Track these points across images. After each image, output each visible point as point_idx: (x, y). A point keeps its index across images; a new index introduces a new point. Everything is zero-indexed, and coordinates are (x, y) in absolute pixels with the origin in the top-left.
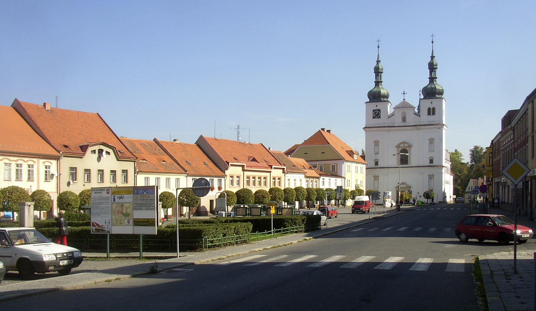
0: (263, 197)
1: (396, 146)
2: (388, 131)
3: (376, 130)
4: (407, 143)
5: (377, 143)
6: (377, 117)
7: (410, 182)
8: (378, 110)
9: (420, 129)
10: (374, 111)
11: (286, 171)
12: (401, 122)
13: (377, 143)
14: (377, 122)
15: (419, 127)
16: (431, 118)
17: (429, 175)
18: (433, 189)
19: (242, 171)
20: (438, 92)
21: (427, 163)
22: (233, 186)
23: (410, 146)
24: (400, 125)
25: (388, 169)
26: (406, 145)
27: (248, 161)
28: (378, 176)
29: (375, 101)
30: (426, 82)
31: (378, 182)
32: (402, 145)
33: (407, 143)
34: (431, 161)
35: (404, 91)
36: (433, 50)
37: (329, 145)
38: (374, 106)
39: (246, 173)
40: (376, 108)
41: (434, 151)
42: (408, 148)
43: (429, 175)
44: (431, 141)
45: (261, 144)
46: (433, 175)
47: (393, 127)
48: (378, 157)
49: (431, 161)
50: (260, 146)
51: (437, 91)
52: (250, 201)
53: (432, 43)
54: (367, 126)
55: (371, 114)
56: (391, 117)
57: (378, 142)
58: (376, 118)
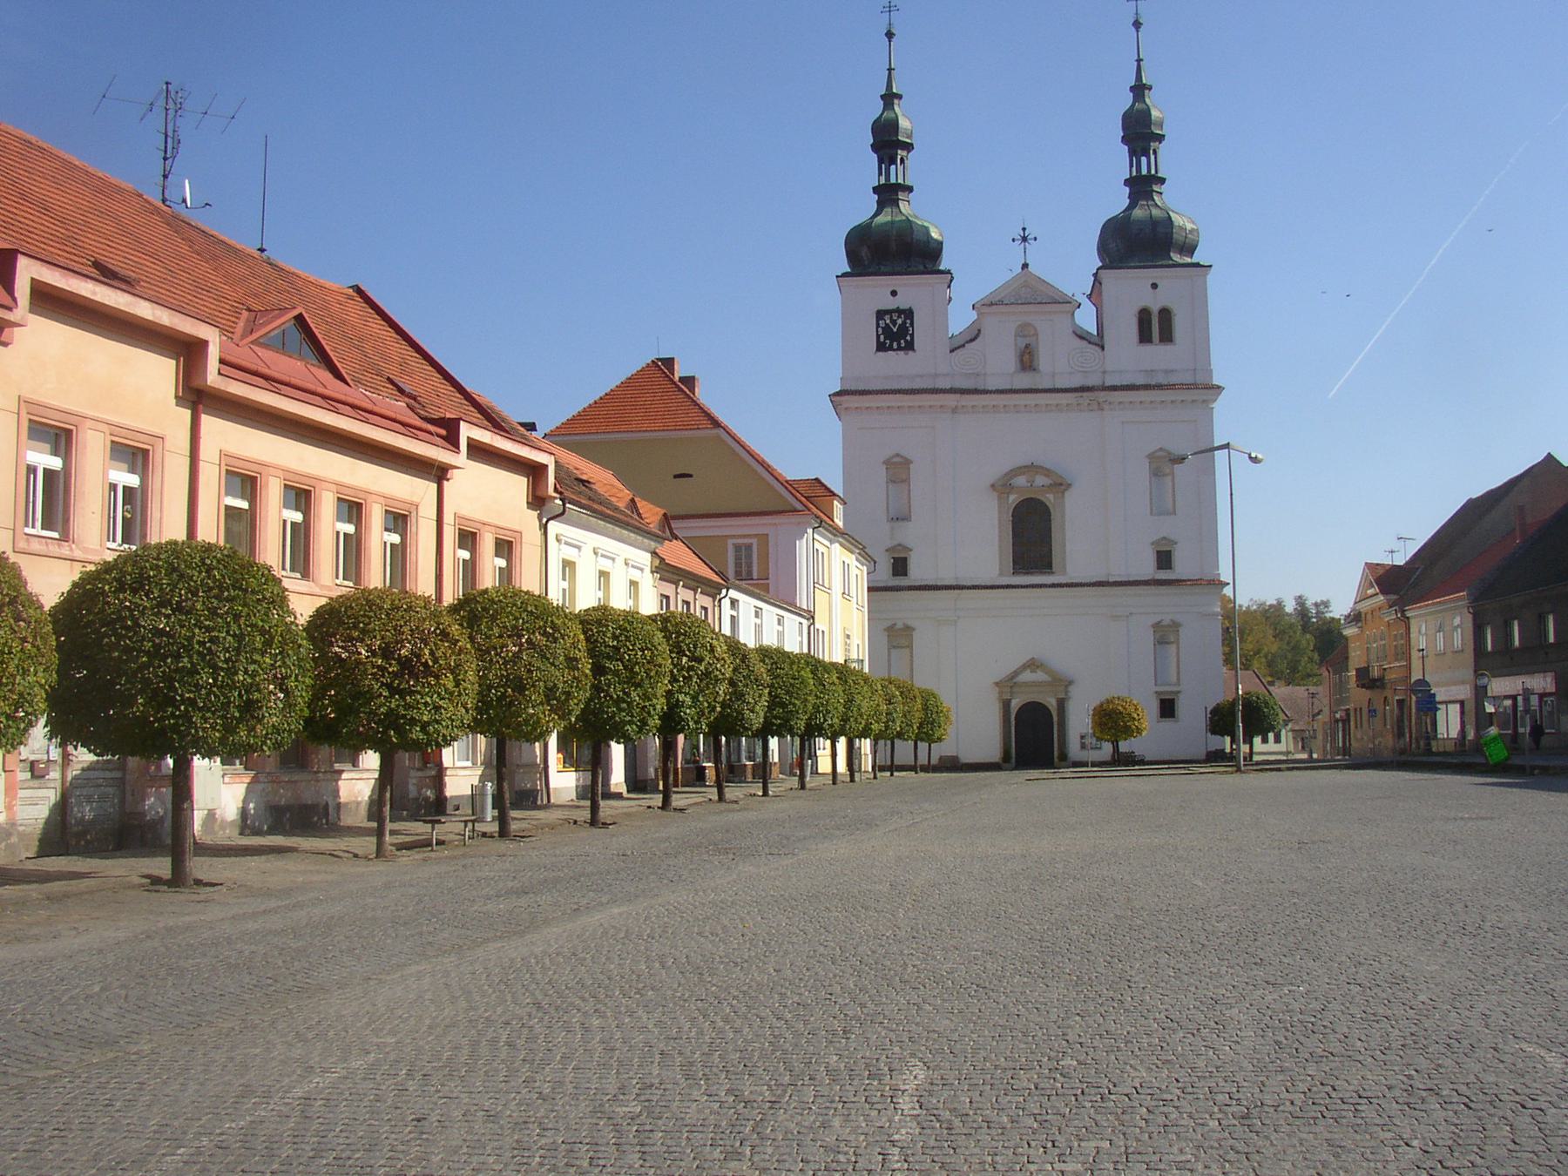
0: (405, 664)
1: (993, 486)
2: (955, 410)
3: (882, 408)
4: (1047, 472)
5: (898, 469)
6: (895, 345)
7: (1063, 659)
8: (899, 311)
9: (1106, 407)
10: (880, 314)
11: (556, 490)
12: (1013, 370)
13: (898, 469)
14: (895, 365)
15: (1102, 395)
16: (1157, 357)
17: (1154, 626)
18: (1179, 692)
19: (180, 401)
20: (1182, 239)
21: (1146, 567)
22: (65, 537)
23: (1061, 486)
24: (1009, 387)
25: (957, 591)
26: (1041, 480)
27: (243, 337)
28: (908, 630)
29: (883, 269)
30: (1118, 201)
31: (912, 653)
32: (1021, 481)
33: (1048, 470)
34: (1164, 559)
35: (1024, 229)
36: (1139, 61)
37: (715, 431)
38: (879, 292)
39: (221, 434)
40: (891, 303)
41: (1174, 513)
42: (1051, 497)
43: (1157, 626)
44: (1164, 463)
45: (359, 291)
46: (1175, 626)
47: (976, 391)
48: (909, 535)
49: (1164, 559)
50: (351, 298)
51: (1175, 236)
52: (250, 708)
53: (1133, 29)
54: (848, 387)
55: (869, 333)
56: (963, 346)
57: (907, 463)
58: (891, 348)
